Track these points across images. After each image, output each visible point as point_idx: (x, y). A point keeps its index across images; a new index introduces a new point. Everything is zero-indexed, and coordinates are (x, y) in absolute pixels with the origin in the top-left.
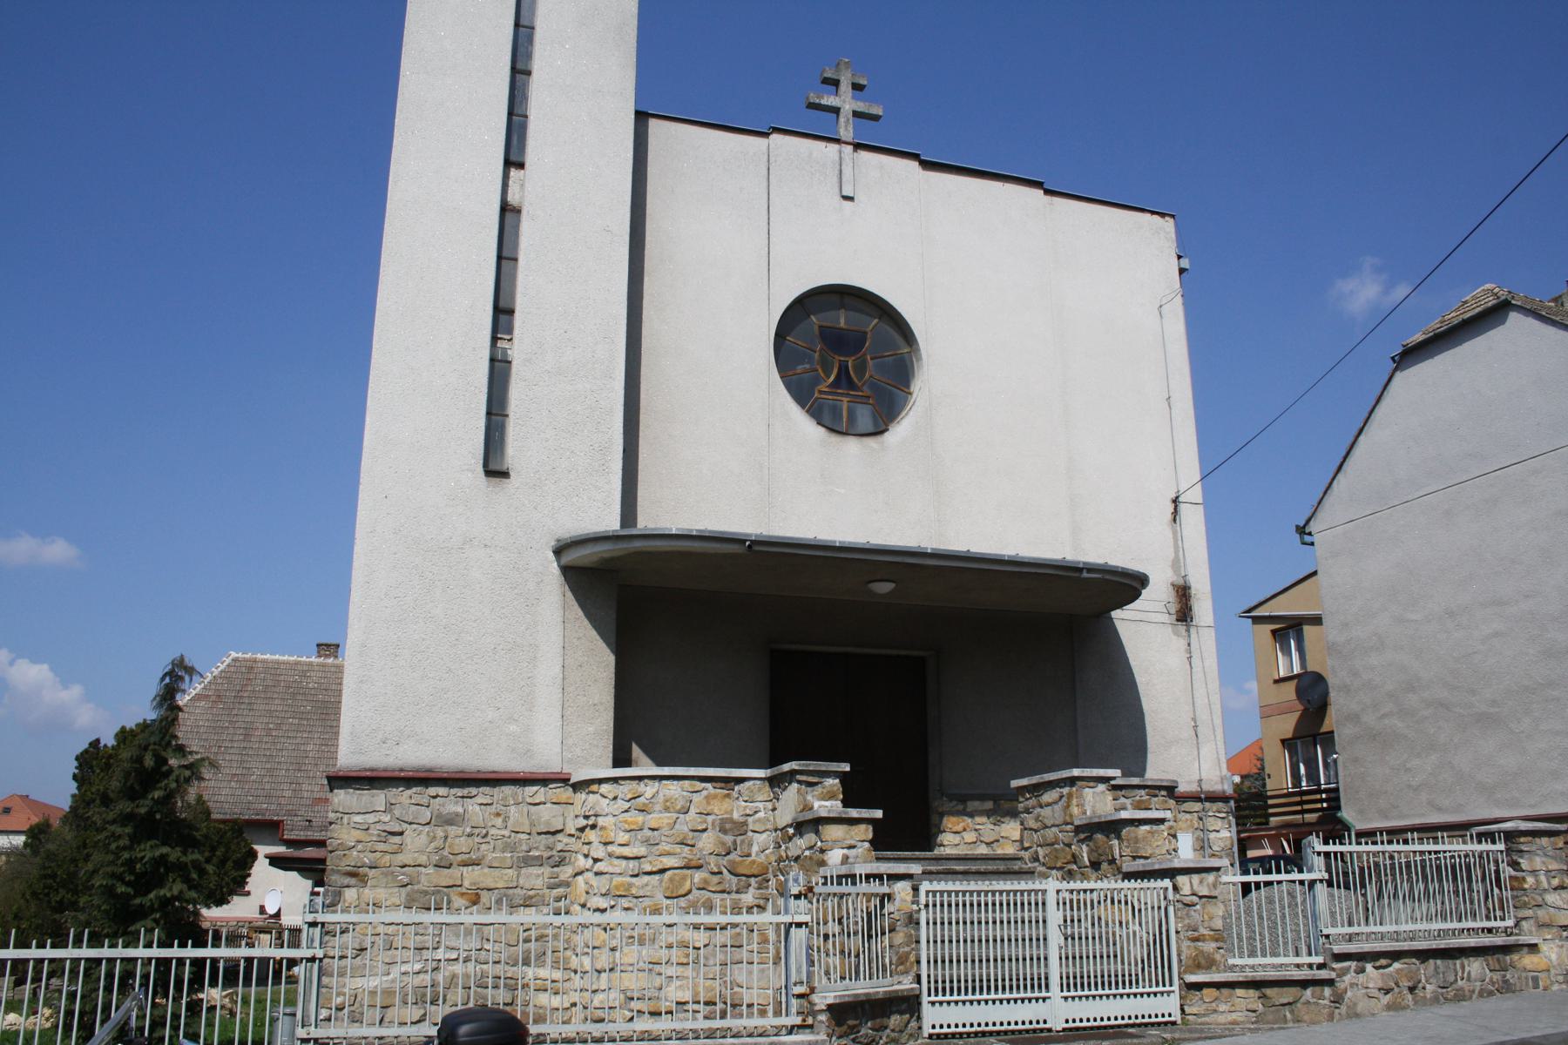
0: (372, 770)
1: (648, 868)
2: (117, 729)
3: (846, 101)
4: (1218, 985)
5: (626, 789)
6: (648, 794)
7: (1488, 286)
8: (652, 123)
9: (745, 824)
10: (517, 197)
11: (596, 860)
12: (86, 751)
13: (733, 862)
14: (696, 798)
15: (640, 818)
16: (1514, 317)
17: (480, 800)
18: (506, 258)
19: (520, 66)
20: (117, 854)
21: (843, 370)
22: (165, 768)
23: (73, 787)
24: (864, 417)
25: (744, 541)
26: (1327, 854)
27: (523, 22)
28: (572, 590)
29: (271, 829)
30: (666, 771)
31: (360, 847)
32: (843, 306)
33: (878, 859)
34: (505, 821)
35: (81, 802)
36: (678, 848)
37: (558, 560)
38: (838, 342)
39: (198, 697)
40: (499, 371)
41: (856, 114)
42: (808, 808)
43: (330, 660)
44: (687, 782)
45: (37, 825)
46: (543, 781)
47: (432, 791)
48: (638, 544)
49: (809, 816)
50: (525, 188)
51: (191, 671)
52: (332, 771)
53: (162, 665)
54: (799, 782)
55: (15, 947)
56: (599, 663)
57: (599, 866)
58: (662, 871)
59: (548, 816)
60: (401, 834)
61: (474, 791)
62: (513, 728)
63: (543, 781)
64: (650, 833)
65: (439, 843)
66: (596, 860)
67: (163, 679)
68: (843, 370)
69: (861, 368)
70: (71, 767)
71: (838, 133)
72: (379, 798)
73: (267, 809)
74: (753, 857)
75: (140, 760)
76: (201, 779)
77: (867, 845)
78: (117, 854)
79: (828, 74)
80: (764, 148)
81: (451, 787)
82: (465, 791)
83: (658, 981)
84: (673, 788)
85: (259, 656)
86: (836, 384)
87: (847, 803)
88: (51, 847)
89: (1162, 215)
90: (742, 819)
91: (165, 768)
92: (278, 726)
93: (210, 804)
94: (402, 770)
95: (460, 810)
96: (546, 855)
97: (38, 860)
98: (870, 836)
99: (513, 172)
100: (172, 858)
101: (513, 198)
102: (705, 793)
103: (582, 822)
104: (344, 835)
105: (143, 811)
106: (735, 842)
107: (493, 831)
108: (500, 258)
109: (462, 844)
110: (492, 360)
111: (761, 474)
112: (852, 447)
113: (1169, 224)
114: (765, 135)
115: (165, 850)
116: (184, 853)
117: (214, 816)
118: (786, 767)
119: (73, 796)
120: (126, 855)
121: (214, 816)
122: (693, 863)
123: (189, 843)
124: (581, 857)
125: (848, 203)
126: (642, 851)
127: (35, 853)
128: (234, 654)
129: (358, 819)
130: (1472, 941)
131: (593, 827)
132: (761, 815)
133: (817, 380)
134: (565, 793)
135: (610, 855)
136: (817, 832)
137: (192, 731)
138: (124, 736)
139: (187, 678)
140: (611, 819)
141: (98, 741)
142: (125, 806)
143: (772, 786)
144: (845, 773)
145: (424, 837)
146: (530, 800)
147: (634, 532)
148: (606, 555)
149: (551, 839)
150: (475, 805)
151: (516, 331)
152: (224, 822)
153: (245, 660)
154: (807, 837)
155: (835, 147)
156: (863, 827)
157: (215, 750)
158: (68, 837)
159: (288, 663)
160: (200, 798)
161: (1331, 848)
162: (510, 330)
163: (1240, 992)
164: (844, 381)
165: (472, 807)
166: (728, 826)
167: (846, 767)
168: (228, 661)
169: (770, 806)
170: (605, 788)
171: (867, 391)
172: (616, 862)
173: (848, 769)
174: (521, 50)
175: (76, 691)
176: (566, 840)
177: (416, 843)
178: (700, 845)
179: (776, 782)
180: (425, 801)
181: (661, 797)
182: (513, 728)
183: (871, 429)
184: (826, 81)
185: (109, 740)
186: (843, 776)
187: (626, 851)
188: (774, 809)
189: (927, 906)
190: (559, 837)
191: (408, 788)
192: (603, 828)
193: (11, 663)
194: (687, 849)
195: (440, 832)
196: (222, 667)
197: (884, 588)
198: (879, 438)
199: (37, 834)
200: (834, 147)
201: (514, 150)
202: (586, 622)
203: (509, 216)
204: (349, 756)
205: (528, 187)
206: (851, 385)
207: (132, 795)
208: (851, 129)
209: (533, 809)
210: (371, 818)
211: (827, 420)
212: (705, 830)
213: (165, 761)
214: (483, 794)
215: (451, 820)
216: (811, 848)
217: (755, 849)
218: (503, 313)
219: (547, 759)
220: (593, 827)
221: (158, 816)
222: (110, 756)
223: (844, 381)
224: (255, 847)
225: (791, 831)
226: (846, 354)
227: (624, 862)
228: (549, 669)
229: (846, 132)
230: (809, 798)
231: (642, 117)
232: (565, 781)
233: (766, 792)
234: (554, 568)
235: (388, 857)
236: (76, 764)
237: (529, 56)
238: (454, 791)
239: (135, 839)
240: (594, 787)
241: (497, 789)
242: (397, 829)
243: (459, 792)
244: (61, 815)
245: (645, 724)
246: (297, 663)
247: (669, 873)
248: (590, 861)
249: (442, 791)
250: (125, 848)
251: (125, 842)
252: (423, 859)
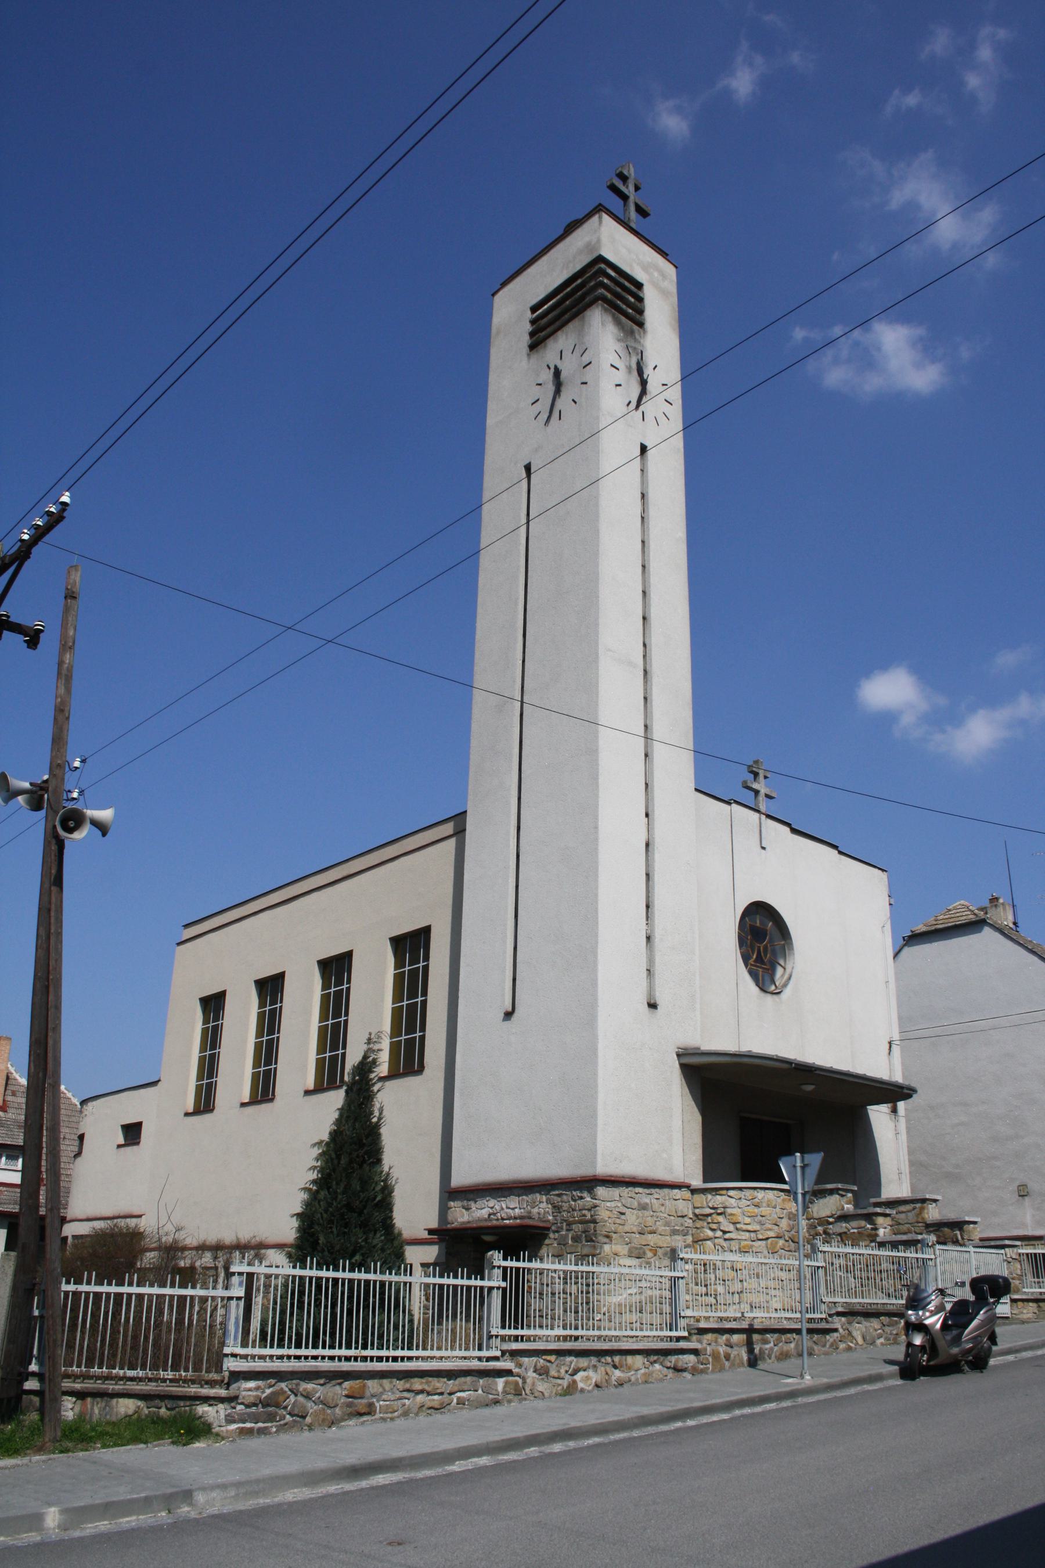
1: (761, 1237)
4: (1023, 1300)
7: (962, 902)
15: (756, 1210)
16: (987, 930)
26: (505, 1269)
47: (638, 1190)
55: (179, 1287)
57: (727, 1236)
58: (767, 1239)
62: (665, 1155)
83: (769, 1297)
84: (770, 1195)
89: (883, 870)
95: (648, 1201)
104: (603, 1214)
113: (884, 876)
114: (728, 803)
126: (757, 1227)
129: (608, 1204)
130: (635, 1346)
145: (634, 1217)
161: (508, 1263)
163: (1031, 1304)
177: (632, 1219)
187: (749, 1228)
189: (547, 1285)
190: (686, 1219)
210: (613, 1204)
226: (763, 937)
227: (747, 1234)
228: (677, 1123)
232: (688, 1187)
243: (647, 1191)
247: (770, 1241)
252: (635, 1229)
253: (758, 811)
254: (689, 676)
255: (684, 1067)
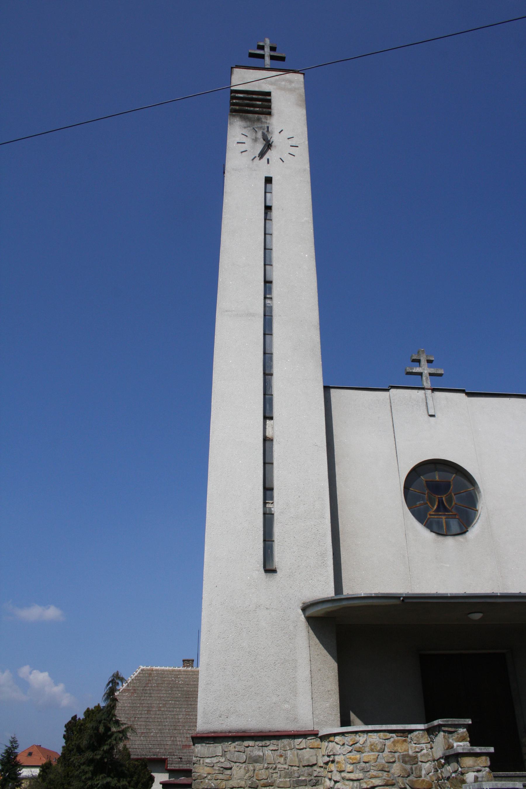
0: (214, 732)
2: (85, 709)
3: (425, 369)
5: (348, 739)
6: (361, 742)
8: (333, 392)
9: (416, 757)
10: (271, 433)
11: (336, 782)
12: (70, 722)
13: (412, 781)
14: (388, 743)
15: (358, 756)
17: (271, 747)
18: (267, 463)
19: (267, 372)
20: (85, 782)
21: (441, 502)
22: (109, 733)
23: (63, 742)
24: (455, 526)
25: (400, 597)
27: (267, 352)
28: (312, 629)
29: (160, 763)
30: (370, 727)
31: (209, 777)
32: (436, 470)
33: (496, 778)
34: (285, 760)
35: (67, 750)
36: (380, 774)
37: (304, 613)
38: (437, 488)
39: (125, 691)
40: (268, 519)
41: (431, 374)
42: (451, 747)
43: (190, 669)
44: (382, 734)
45: (45, 764)
46: (304, 735)
47: (246, 743)
48: (345, 603)
49: (451, 752)
50: (275, 428)
51: (122, 680)
52: (194, 735)
53: (108, 678)
54: (444, 731)
56: (329, 667)
59: (308, 755)
60: (230, 769)
61: (268, 743)
62: (286, 706)
63: (304, 735)
64: (364, 765)
65: (250, 773)
66: (336, 782)
67: (108, 684)
68: (441, 502)
69: (450, 500)
70: (62, 731)
71: (423, 385)
72: (218, 748)
73: (160, 752)
74: (423, 778)
75: (97, 729)
76: (127, 738)
77: (487, 769)
78: (85, 782)
79: (415, 357)
80: (388, 397)
81: (256, 741)
82: (263, 743)
84: (375, 738)
85: (154, 668)
86: (438, 510)
87: (473, 744)
88: (52, 776)
90: (414, 755)
91: (109, 733)
92: (164, 705)
93: (130, 750)
94: (230, 732)
95: (261, 754)
96: (308, 779)
97: (45, 784)
98: (489, 763)
99: (268, 422)
100: (112, 784)
101: (269, 434)
102: (392, 739)
103: (326, 759)
105: (98, 757)
106: (412, 769)
107: (279, 766)
108: (265, 463)
109: (263, 774)
110: (264, 514)
111: (405, 562)
112: (450, 541)
114: (387, 390)
115: (109, 779)
116: (119, 781)
117: (132, 757)
118: (436, 723)
119: (63, 747)
120: (89, 783)
121: (132, 757)
122: (390, 782)
123: (121, 775)
124: (327, 780)
125: (432, 419)
126: (360, 775)
127: (44, 780)
128: (142, 667)
129: (208, 760)
131: (333, 762)
132: (425, 751)
133: (427, 509)
134: (316, 742)
135: (343, 778)
136: (458, 762)
137: (122, 714)
138: (89, 713)
139: (120, 683)
140: (342, 757)
141: (76, 716)
142: (89, 755)
143: (429, 734)
144: (469, 725)
145: (242, 772)
146: (297, 747)
147: (342, 597)
148: (328, 610)
149: (310, 769)
150: (268, 751)
151: (275, 499)
152: (137, 760)
153: (148, 670)
154: (452, 764)
155: (422, 392)
156: (484, 758)
157: (132, 719)
158: (60, 771)
159: (169, 671)
160: (125, 745)
162: (272, 498)
164: (442, 508)
165: (268, 752)
166: (407, 759)
167: (492, 750)
168: (139, 671)
169: (429, 746)
170: (337, 739)
171: (454, 512)
172: (347, 782)
173: (470, 722)
174: (267, 364)
175: (60, 687)
176: (319, 770)
178: (392, 771)
179: (431, 732)
180: (242, 749)
181: (368, 743)
182: (286, 706)
183: (459, 532)
184: (414, 361)
185: (81, 716)
186: (468, 727)
187: (352, 776)
188: (431, 748)
190: (315, 768)
191: (234, 742)
192: (338, 762)
193: (30, 673)
194: (385, 773)
195: (251, 767)
196: (136, 674)
197: (477, 616)
198: (464, 536)
199: (45, 768)
200: (422, 392)
201: (267, 411)
202: (321, 646)
203: (267, 443)
204: (204, 724)
205: (276, 428)
206: (446, 510)
207: (93, 748)
208: (429, 382)
209: (300, 752)
210: (215, 760)
211: (435, 528)
212: (394, 762)
213: (109, 729)
214: (273, 744)
215: (256, 760)
216: (455, 772)
217: (423, 772)
218: (268, 490)
219: (305, 721)
220: (333, 762)
221: (106, 760)
222: (82, 725)
223: (442, 508)
224: (153, 774)
225: (443, 761)
226: (441, 495)
227: (351, 783)
228: (303, 673)
229: (427, 383)
230: (451, 741)
231: (327, 389)
232: (315, 734)
233: (426, 738)
234: (302, 618)
235: (224, 782)
236: (65, 729)
237: (271, 367)
238: (257, 743)
239: (95, 773)
240: (332, 738)
241: (280, 742)
242: (228, 766)
243: (260, 743)
244: (57, 757)
245: (356, 701)
246: (173, 671)
248: (333, 783)
249: (251, 743)
250: (89, 779)
251: (89, 775)
253: (423, 389)
254: (316, 308)
255: (311, 620)
